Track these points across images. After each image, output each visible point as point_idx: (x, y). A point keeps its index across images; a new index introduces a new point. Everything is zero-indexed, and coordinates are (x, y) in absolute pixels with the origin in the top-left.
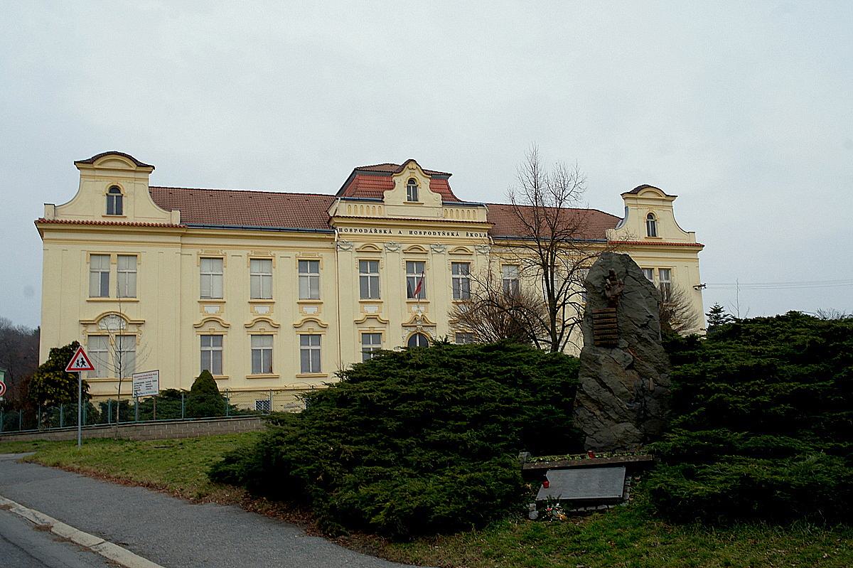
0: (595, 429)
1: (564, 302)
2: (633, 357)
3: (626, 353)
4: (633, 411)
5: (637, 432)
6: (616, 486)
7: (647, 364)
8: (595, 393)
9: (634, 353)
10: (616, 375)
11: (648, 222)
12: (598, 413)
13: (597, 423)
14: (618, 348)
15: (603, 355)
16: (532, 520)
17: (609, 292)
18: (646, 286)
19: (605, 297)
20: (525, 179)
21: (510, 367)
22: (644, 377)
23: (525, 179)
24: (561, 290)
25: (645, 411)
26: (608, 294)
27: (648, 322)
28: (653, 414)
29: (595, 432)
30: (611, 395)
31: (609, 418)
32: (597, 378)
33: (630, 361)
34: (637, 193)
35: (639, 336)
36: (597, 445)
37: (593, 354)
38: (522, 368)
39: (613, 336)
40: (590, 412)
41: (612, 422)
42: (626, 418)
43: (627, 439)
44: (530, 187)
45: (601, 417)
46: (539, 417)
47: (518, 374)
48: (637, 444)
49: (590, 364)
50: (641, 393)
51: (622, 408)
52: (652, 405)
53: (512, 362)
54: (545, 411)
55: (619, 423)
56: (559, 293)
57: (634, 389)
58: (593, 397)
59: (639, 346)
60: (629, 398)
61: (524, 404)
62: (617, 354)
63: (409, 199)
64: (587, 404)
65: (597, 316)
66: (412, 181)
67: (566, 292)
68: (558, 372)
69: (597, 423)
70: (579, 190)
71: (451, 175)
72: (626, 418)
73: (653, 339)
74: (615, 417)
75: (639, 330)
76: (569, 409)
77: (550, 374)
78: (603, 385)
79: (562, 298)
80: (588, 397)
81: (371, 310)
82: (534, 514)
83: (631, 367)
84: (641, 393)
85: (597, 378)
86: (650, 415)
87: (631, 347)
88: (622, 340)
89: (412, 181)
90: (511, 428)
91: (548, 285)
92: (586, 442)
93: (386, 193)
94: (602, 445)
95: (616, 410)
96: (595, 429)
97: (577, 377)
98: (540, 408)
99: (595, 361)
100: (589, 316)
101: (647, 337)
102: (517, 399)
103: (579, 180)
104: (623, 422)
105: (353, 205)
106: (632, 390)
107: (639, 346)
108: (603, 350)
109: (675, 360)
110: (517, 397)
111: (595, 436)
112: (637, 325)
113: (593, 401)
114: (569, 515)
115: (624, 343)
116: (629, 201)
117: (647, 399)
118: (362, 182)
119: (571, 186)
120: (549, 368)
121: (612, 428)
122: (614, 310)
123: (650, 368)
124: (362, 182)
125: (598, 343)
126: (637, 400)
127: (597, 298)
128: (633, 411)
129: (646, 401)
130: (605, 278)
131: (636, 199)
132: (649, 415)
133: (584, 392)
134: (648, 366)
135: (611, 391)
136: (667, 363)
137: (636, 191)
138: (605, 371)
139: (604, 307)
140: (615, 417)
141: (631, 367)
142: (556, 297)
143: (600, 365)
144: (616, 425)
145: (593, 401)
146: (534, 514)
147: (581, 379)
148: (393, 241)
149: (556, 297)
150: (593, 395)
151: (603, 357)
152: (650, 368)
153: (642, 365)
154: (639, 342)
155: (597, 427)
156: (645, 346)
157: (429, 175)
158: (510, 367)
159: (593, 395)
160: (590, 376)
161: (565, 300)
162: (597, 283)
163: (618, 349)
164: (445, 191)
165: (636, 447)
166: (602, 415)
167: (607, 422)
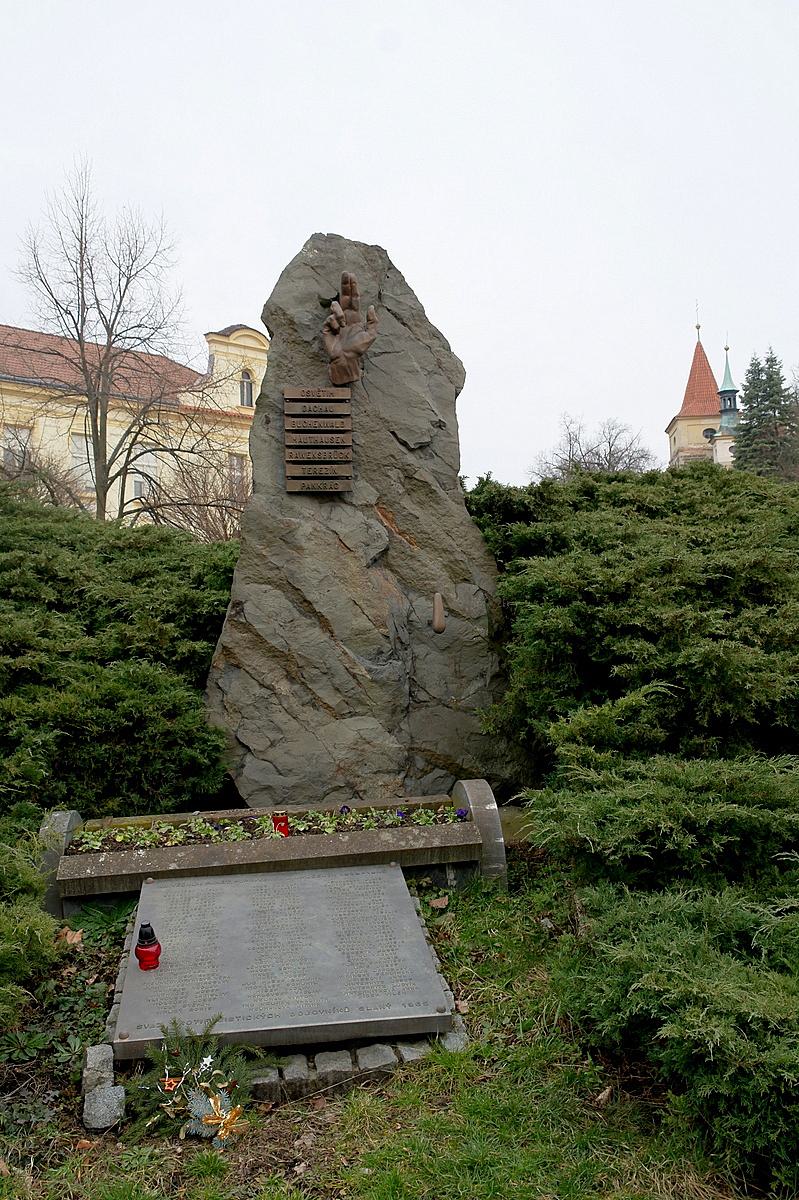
0: (273, 735)
1: (126, 466)
2: (390, 531)
3: (372, 521)
4: (383, 684)
5: (391, 743)
6: (403, 953)
7: (424, 555)
8: (280, 631)
9: (392, 521)
10: (344, 580)
12: (284, 687)
13: (281, 718)
14: (351, 504)
15: (307, 519)
16: (98, 1132)
17: (336, 339)
18: (428, 342)
19: (322, 357)
20: (62, 220)
21: (21, 554)
22: (415, 590)
23: (62, 220)
24: (120, 445)
25: (413, 682)
26: (334, 345)
28: (434, 692)
29: (273, 744)
30: (325, 637)
31: (315, 703)
32: (290, 588)
33: (381, 544)
34: (228, 336)
36: (275, 780)
37: (280, 517)
39: (342, 470)
40: (262, 685)
41: (321, 715)
42: (361, 703)
43: (362, 763)
44: (71, 240)
45: (292, 699)
46: (110, 701)
47: (45, 574)
48: (386, 778)
49: (269, 544)
50: (404, 635)
51: (354, 676)
52: (433, 668)
53: (24, 540)
54: (130, 680)
55: (343, 716)
56: (117, 450)
57: (390, 623)
58: (274, 642)
59: (406, 502)
60: (372, 649)
61: (65, 655)
62: (347, 521)
64: (255, 661)
65: (298, 408)
67: (130, 450)
68: (156, 572)
69: (281, 718)
70: (164, 263)
72: (361, 703)
73: (442, 485)
74: (334, 700)
75: (410, 458)
76: (197, 670)
77: (136, 579)
78: (306, 607)
79: (122, 459)
80: (258, 641)
82: (105, 1103)
83: (381, 559)
84: (404, 635)
85: (290, 588)
86: (426, 698)
87: (384, 505)
88: (361, 483)
90: (20, 735)
91: (94, 421)
92: (245, 771)
94: (291, 780)
95: (337, 681)
96: (273, 735)
97: (228, 583)
98: (118, 669)
99: (286, 538)
100: (272, 407)
101: (430, 479)
102: (45, 642)
103: (164, 245)
104: (352, 714)
106: (384, 625)
108: (306, 507)
109: (506, 554)
110: (44, 634)
111: (272, 754)
112: (404, 444)
113: (274, 654)
114: (256, 1097)
116: (215, 347)
117: (420, 650)
119: (149, 253)
120: (136, 564)
121: (322, 730)
122: (344, 393)
123: (432, 565)
125: (296, 486)
126: (393, 655)
127: (298, 358)
128: (383, 684)
129: (414, 658)
130: (326, 304)
131: (228, 344)
132: (422, 696)
133: (247, 627)
135: (324, 623)
136: (476, 554)
137: (227, 333)
138: (313, 568)
139: (319, 386)
140: (334, 700)
141: (381, 559)
142: (108, 458)
143: (299, 549)
144: (334, 725)
145: (274, 654)
146: (105, 1103)
147: (241, 588)
149: (108, 458)
150: (275, 635)
151: (307, 527)
152: (432, 565)
153: (412, 557)
154: (408, 492)
155: (279, 730)
156: (421, 504)
158: (21, 554)
159: (275, 635)
161: (128, 462)
162: (303, 314)
163: (348, 509)
165: (385, 785)
166: (294, 694)
167: (309, 714)
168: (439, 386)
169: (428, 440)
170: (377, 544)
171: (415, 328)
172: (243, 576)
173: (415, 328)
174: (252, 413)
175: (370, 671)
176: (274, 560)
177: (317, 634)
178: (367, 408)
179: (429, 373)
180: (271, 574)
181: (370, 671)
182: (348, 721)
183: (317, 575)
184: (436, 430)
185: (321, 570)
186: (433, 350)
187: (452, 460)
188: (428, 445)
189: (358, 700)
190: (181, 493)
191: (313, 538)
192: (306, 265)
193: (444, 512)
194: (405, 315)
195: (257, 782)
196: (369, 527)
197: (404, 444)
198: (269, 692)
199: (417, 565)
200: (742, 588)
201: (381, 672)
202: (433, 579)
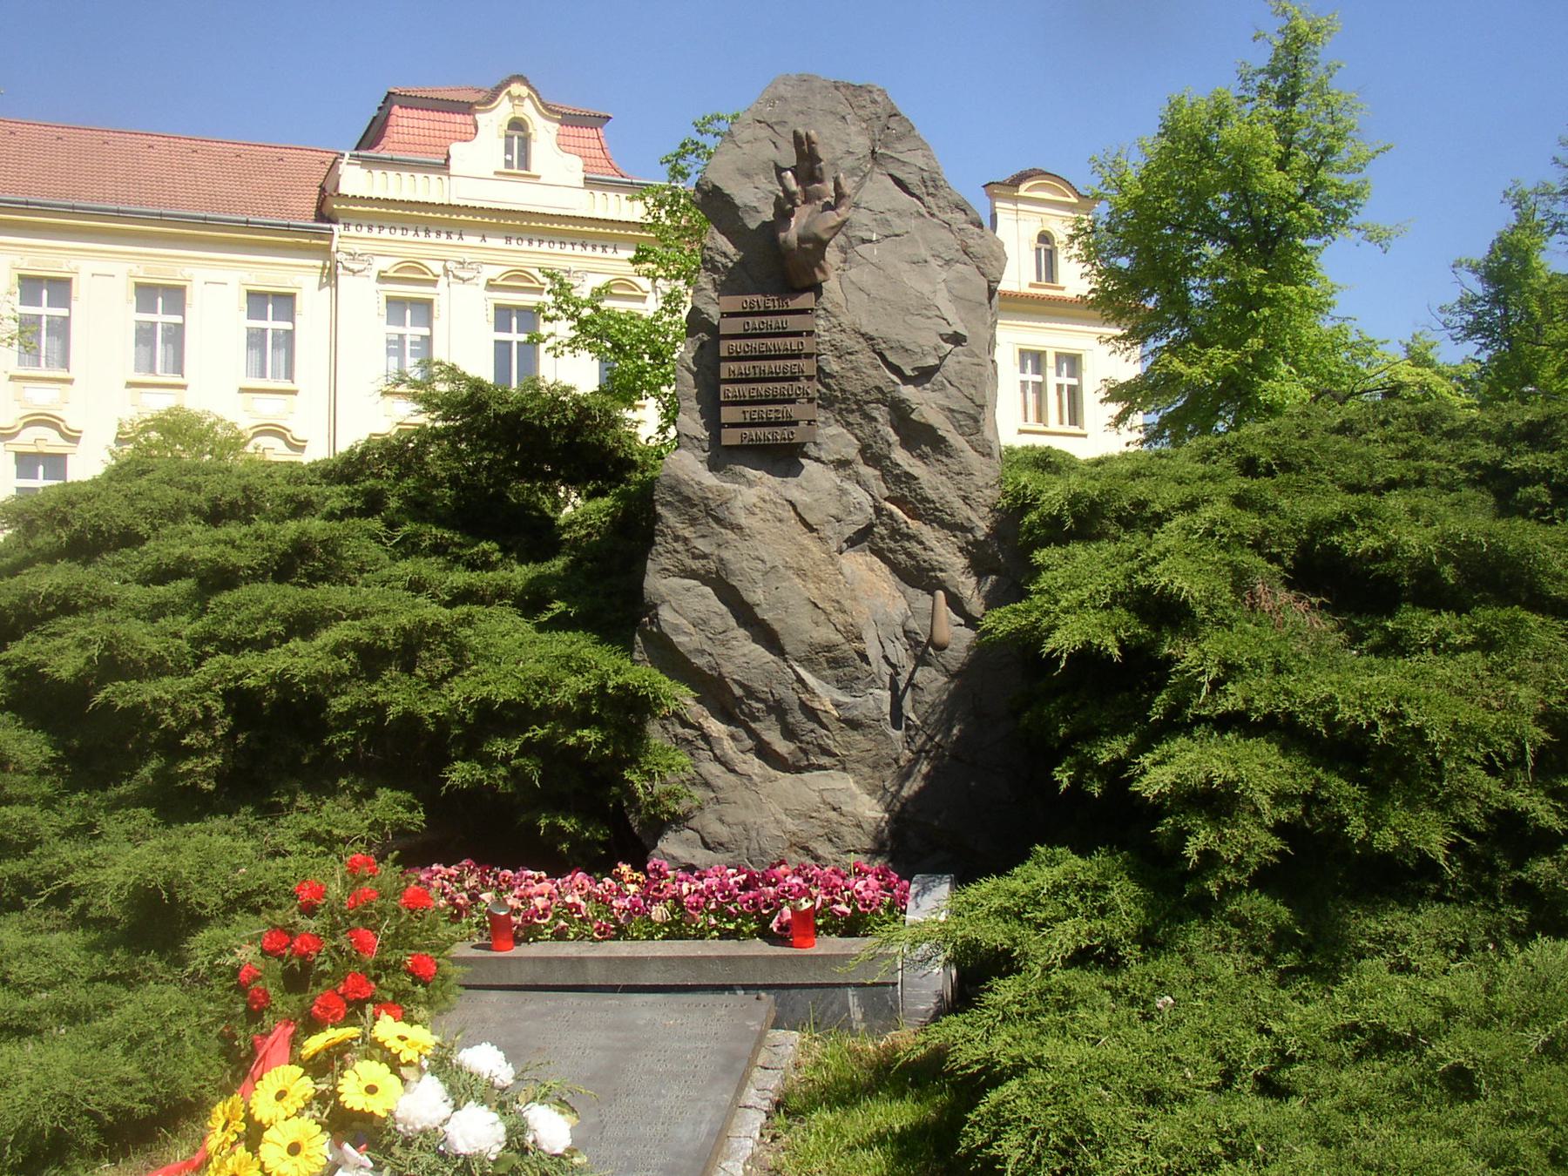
3: (848, 485)
7: (928, 533)
10: (801, 573)
11: (1038, 250)
12: (715, 727)
18: (947, 217)
27: (942, 359)
35: (900, 414)
38: (1406, 631)
42: (826, 752)
49: (693, 521)
63: (508, 164)
66: (517, 125)
71: (609, 118)
75: (907, 392)
78: (745, 614)
81: (43, 398)
89: (517, 125)
93: (456, 149)
104: (811, 767)
105: (377, 173)
107: (900, 456)
112: (896, 370)
115: (835, 438)
118: (405, 122)
124: (405, 122)
134: (932, 543)
140: (782, 746)
148: (468, 257)
156: (923, 457)
157: (557, 112)
160: (692, 574)
164: (593, 153)
168: (963, 279)
169: (932, 361)
170: (855, 518)
171: (927, 199)
172: (659, 568)
173: (927, 199)
174: (723, 387)
175: (837, 705)
176: (702, 545)
177: (759, 652)
178: (842, 319)
179: (947, 262)
180: (696, 565)
181: (837, 705)
182: (806, 776)
183: (760, 566)
184: (949, 347)
185: (766, 558)
186: (954, 227)
187: (973, 392)
188: (934, 370)
189: (819, 746)
190: (1043, 866)
191: (757, 511)
192: (760, 122)
193: (956, 468)
194: (912, 179)
195: (674, 858)
196: (843, 492)
197: (896, 370)
198: (695, 733)
199: (915, 548)
200: (1159, 183)
201: (855, 707)
202: (941, 570)
